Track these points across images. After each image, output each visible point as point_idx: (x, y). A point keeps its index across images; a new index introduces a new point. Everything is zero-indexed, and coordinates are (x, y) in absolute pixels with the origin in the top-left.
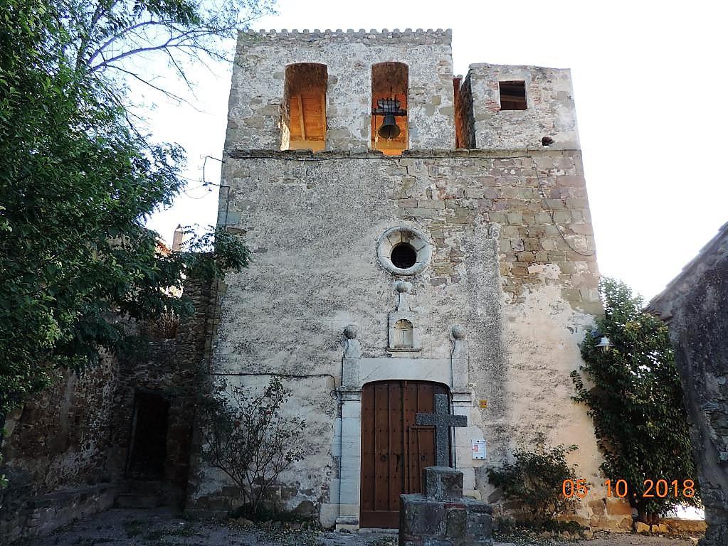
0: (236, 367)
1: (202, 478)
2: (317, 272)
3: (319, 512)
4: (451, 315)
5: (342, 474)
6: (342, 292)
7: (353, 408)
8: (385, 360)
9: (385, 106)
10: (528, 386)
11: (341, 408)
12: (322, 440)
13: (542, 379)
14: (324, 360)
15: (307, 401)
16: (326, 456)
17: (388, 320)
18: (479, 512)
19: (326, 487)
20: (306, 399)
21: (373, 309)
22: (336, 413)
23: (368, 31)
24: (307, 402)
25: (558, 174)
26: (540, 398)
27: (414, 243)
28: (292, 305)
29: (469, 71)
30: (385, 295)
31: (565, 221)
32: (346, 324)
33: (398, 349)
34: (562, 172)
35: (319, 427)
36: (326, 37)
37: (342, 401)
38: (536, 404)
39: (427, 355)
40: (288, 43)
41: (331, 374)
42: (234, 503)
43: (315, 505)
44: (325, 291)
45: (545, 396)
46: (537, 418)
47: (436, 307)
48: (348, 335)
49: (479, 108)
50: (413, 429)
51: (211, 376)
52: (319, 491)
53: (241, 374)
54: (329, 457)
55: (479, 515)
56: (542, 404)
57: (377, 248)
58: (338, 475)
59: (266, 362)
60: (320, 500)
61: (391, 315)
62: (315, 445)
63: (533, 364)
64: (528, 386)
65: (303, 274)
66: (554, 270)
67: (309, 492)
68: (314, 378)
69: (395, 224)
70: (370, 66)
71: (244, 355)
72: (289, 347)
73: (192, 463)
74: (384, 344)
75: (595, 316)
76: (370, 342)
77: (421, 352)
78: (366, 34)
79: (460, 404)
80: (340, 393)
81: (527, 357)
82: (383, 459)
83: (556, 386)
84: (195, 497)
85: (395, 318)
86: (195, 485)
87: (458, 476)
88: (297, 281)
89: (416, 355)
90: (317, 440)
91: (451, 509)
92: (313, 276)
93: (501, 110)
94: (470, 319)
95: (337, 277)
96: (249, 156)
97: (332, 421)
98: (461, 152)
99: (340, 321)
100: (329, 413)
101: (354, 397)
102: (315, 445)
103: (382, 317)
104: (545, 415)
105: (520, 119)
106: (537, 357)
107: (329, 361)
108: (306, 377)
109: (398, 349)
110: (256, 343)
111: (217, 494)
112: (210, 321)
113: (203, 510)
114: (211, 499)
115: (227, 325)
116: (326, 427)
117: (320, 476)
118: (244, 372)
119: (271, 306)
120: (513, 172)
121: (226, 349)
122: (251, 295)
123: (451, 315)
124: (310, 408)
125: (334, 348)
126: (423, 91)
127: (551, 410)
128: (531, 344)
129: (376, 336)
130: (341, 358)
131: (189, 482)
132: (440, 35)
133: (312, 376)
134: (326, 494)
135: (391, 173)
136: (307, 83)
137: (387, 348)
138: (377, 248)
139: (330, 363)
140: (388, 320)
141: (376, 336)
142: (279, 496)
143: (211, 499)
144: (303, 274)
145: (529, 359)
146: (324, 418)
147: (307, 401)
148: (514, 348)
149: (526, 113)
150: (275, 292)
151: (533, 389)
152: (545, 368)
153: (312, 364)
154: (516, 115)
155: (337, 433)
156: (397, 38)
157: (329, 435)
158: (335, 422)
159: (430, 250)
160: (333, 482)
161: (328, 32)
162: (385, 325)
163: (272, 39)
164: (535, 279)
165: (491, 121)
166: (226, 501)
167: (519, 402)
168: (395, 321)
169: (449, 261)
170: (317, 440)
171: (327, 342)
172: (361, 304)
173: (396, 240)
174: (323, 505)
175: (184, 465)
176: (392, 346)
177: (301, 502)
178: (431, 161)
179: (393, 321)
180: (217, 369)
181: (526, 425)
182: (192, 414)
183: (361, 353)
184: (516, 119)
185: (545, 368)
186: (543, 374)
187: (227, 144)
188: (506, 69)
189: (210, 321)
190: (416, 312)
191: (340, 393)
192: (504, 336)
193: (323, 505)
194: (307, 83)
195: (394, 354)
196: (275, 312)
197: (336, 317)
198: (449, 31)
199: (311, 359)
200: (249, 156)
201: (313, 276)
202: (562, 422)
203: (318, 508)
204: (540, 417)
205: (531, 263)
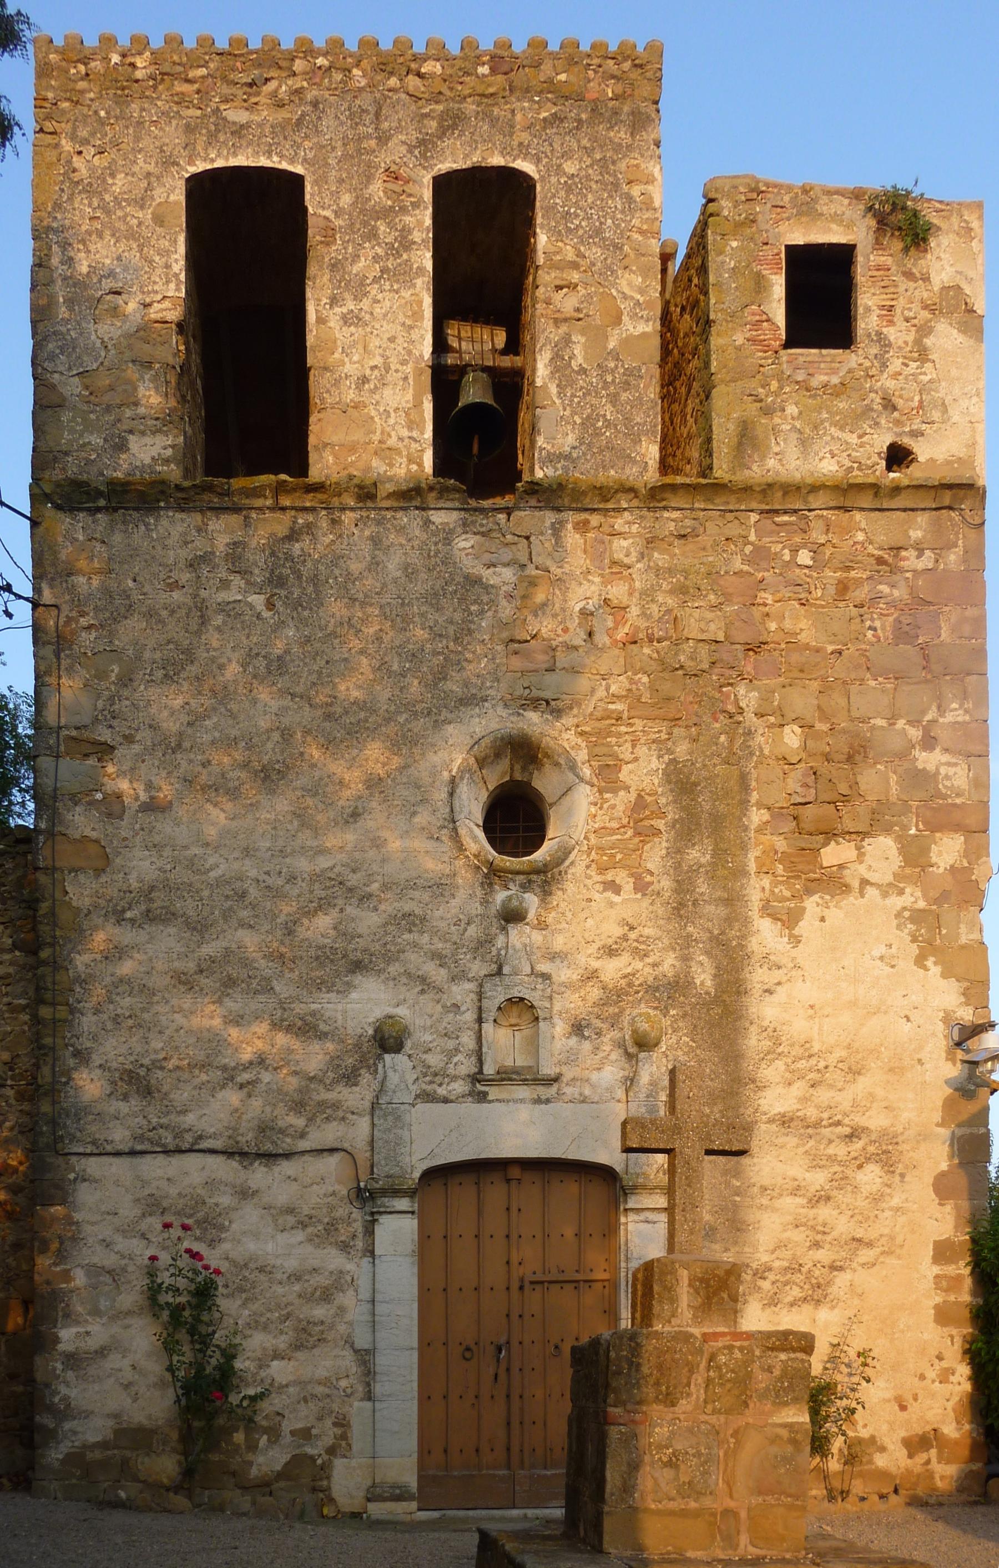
0: (119, 1136)
1: (65, 1412)
2: (303, 865)
3: (328, 1478)
4: (630, 985)
5: (378, 1389)
6: (368, 921)
7: (398, 1230)
8: (470, 1108)
9: (464, 345)
10: (797, 1170)
11: (372, 1233)
12: (332, 1312)
13: (831, 1151)
14: (331, 1111)
15: (292, 1217)
16: (344, 1346)
17: (480, 1000)
18: (784, 1350)
19: (342, 1423)
20: (290, 1211)
21: (443, 972)
22: (360, 1244)
23: (419, 48)
24: (291, 1220)
25: (920, 565)
26: (822, 1198)
27: (546, 783)
28: (246, 963)
29: (705, 206)
30: (472, 931)
31: (924, 712)
32: (378, 1013)
33: (506, 1076)
34: (927, 561)
35: (322, 1280)
36: (299, 65)
37: (372, 1214)
38: (812, 1213)
39: (568, 1090)
40: (186, 88)
41: (346, 1145)
42: (143, 1463)
43: (319, 1462)
44: (324, 922)
45: (835, 1193)
46: (810, 1248)
47: (595, 964)
48: (388, 1040)
49: (728, 342)
50: (532, 1283)
51: (60, 1160)
52: (327, 1433)
53: (133, 1153)
54: (348, 1353)
55: (783, 1356)
56: (824, 1212)
57: (451, 794)
58: (370, 1391)
59: (190, 1119)
60: (332, 1451)
61: (487, 986)
62: (315, 1324)
63: (811, 1113)
64: (797, 1170)
65: (268, 873)
66: (882, 855)
67: (305, 1434)
68: (307, 1158)
69: (491, 721)
70: (427, 179)
71: (135, 1103)
72: (246, 1076)
73: (39, 1376)
74: (466, 1066)
75: (966, 984)
76: (434, 1060)
77: (556, 1086)
78: (415, 58)
79: (643, 1216)
80: (370, 1196)
81: (800, 1094)
82: (468, 1355)
83: (860, 1167)
84: (55, 1455)
85: (496, 995)
86: (52, 1426)
87: (729, 1273)
88: (253, 893)
89: (543, 1092)
90: (319, 1312)
91: (720, 1344)
92: (292, 879)
93: (788, 344)
94: (671, 990)
95: (354, 880)
96: (102, 503)
97: (350, 1267)
98: (673, 488)
99: (365, 1003)
100: (345, 1247)
101: (403, 1204)
102: (315, 1324)
103: (462, 992)
104: (829, 1238)
105: (835, 380)
106: (824, 1095)
107: (340, 1114)
108: (288, 1156)
109: (506, 1076)
110: (162, 1068)
111: (104, 1445)
112: (45, 1012)
113: (74, 1481)
114: (89, 1456)
115: (87, 1022)
116: (340, 1282)
117: (328, 1396)
118: (139, 1147)
119: (191, 966)
120: (804, 557)
121: (89, 1085)
122: (142, 936)
123: (630, 985)
124: (300, 1236)
125: (350, 1078)
126: (575, 277)
127: (843, 1227)
128: (813, 1061)
129: (451, 1044)
130: (367, 1105)
131: (38, 1418)
132: (627, 65)
133: (303, 1153)
134: (344, 1437)
135: (487, 557)
136: (249, 239)
137: (477, 1077)
138: (451, 794)
139: (343, 1119)
140: (480, 1000)
141: (451, 1044)
142: (239, 1445)
143: (89, 1456)
144: (268, 873)
145: (804, 1100)
146: (334, 1259)
147: (292, 1217)
148: (771, 1072)
149: (848, 360)
150: (199, 928)
151: (807, 1175)
152: (838, 1123)
153: (300, 1122)
154: (823, 364)
155: (365, 1294)
156: (514, 69)
157: (347, 1299)
158: (357, 1268)
159: (583, 797)
160: (358, 1409)
161: (306, 49)
162: (470, 1016)
163: (139, 74)
164: (834, 883)
165: (753, 385)
166: (125, 1462)
167: (775, 1210)
168: (497, 1003)
169: (630, 833)
170: (319, 1312)
171: (334, 1062)
172: (412, 957)
173: (496, 776)
174: (339, 1463)
175: (20, 1389)
176: (489, 1070)
177: (289, 1456)
178: (595, 519)
179: (491, 1005)
180: (73, 1138)
181: (786, 1264)
182: (24, 1267)
183: (414, 1089)
184: (824, 378)
185: (838, 1123)
186: (833, 1137)
187: (41, 460)
188: (806, 202)
189: (45, 1012)
190: (546, 977)
191: (370, 1196)
192: (753, 1042)
193: (339, 1463)
194: (249, 239)
195: (493, 1092)
196: (204, 981)
197: (354, 995)
198: (656, 50)
199: (298, 1106)
200: (102, 503)
201: (292, 879)
202: (866, 1255)
203: (325, 1469)
204: (817, 1245)
205: (830, 835)
